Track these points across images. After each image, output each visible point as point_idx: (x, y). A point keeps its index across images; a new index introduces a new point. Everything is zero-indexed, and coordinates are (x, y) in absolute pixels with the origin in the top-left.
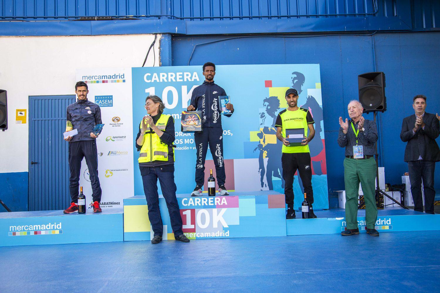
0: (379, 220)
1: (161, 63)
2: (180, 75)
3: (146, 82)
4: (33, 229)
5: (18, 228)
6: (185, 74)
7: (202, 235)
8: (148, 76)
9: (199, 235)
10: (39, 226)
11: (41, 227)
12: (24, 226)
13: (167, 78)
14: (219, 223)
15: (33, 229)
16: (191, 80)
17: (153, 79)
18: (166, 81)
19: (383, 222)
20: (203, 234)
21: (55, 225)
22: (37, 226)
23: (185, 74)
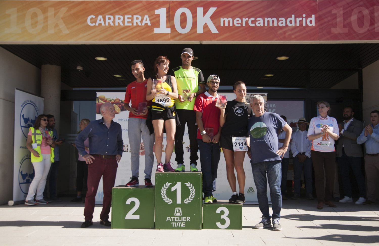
0: (312, 18)
1: (353, 113)
2: (128, 18)
6: (270, 104)
7: (259, 22)
8: (92, 19)
9: (252, 22)
13: (114, 22)
14: (206, 26)
16: (142, 24)
17: (98, 22)
18: (112, 24)
19: (301, 22)
21: (304, 19)
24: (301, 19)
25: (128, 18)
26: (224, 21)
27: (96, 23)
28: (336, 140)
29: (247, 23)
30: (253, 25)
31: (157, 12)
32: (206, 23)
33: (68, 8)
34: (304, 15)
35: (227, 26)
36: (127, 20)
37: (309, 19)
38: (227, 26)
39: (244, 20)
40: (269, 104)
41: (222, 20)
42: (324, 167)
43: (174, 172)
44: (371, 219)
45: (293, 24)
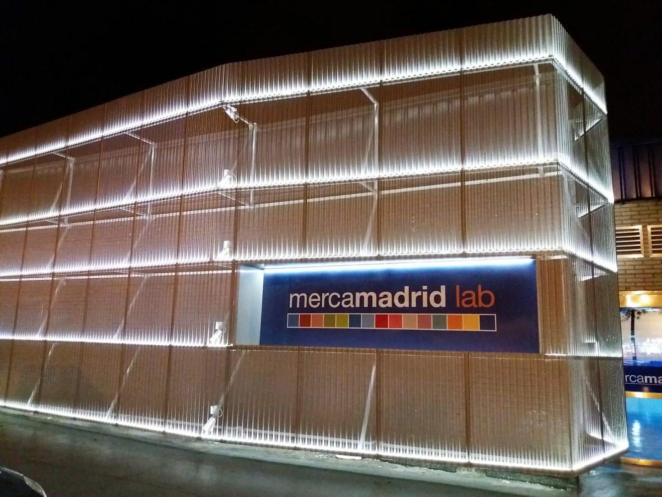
4: (354, 303)
5: (310, 300)
10: (374, 295)
11: (378, 299)
12: (328, 294)
15: (354, 303)
19: (419, 299)
20: (389, 294)
21: (425, 294)
22: (366, 295)
24: (419, 293)
34: (425, 287)
35: (367, 306)
38: (367, 306)
43: (382, 92)
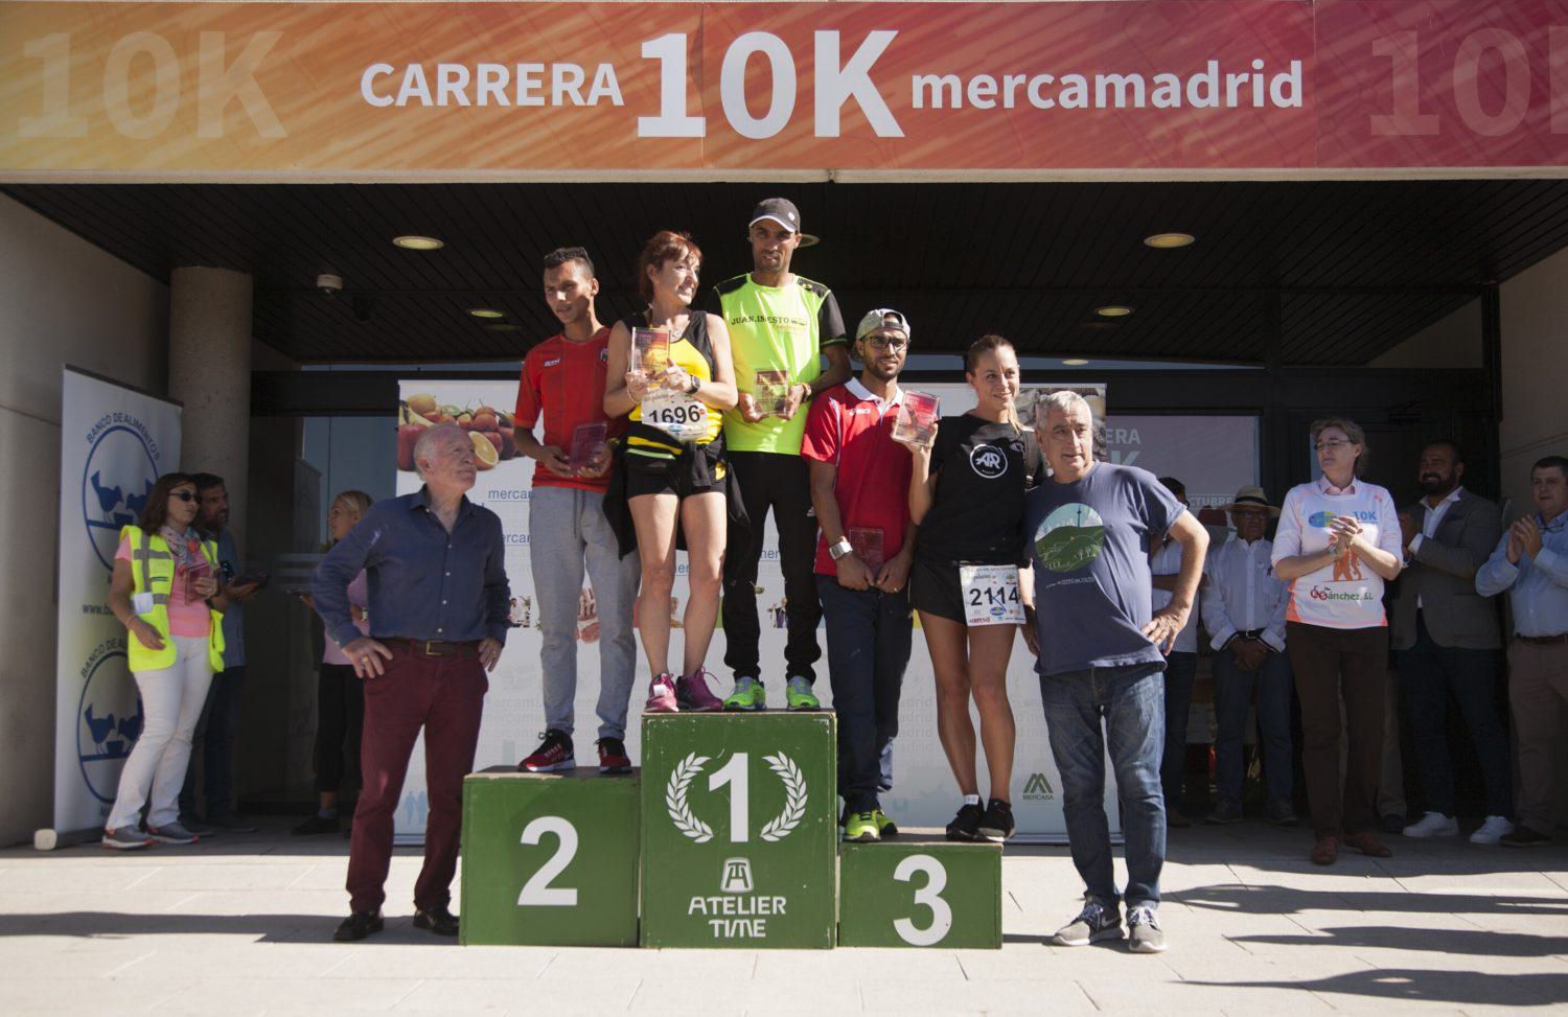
0: (1289, 72)
2: (531, 76)
3: (981, 76)
6: (1118, 431)
8: (379, 77)
9: (1044, 91)
13: (471, 91)
16: (586, 99)
17: (406, 92)
18: (463, 101)
19: (1245, 90)
21: (1258, 79)
23: (558, 69)
24: (1244, 77)
25: (531, 76)
26: (927, 89)
27: (395, 97)
28: (1391, 579)
29: (1021, 93)
30: (1049, 104)
31: (649, 49)
32: (852, 97)
33: (281, 34)
34: (1258, 64)
35: (940, 106)
36: (524, 84)
37: (1278, 80)
38: (940, 106)
39: (1011, 83)
40: (1114, 432)
41: (918, 82)
42: (1339, 690)
44: (1535, 905)
45: (1213, 100)
